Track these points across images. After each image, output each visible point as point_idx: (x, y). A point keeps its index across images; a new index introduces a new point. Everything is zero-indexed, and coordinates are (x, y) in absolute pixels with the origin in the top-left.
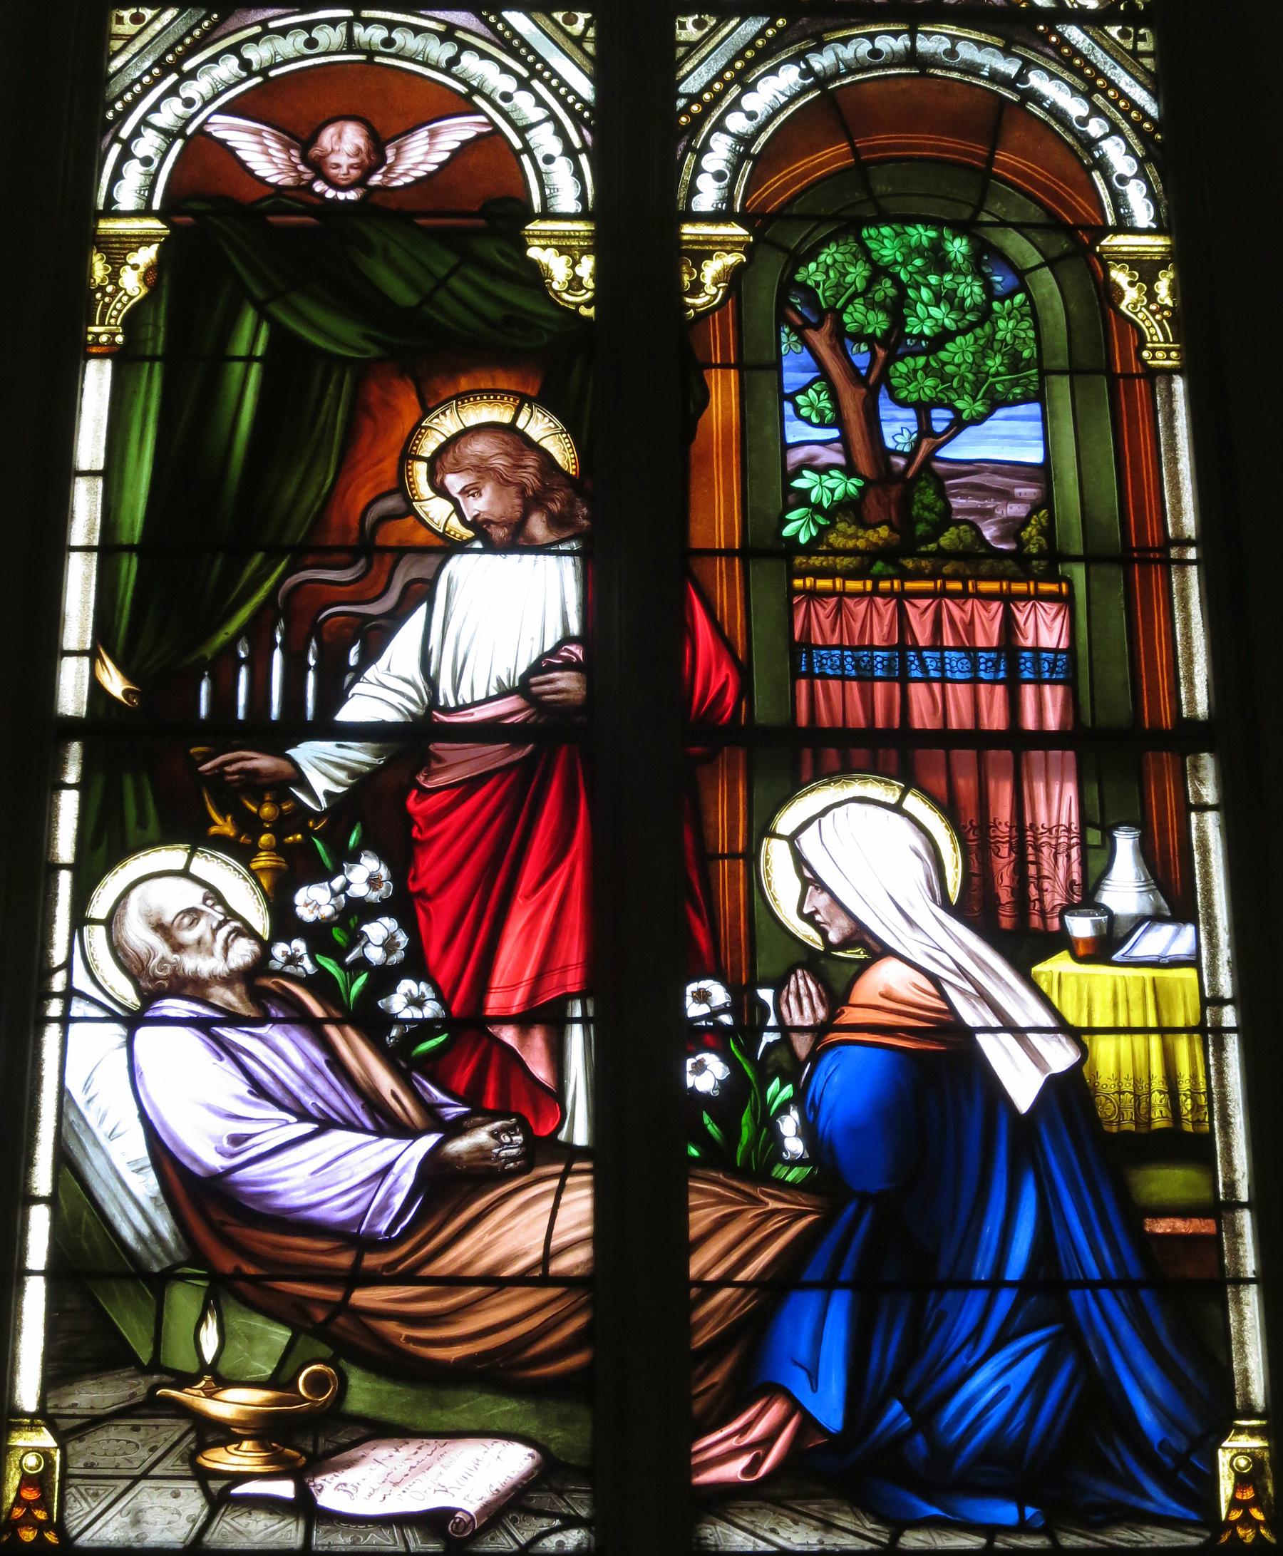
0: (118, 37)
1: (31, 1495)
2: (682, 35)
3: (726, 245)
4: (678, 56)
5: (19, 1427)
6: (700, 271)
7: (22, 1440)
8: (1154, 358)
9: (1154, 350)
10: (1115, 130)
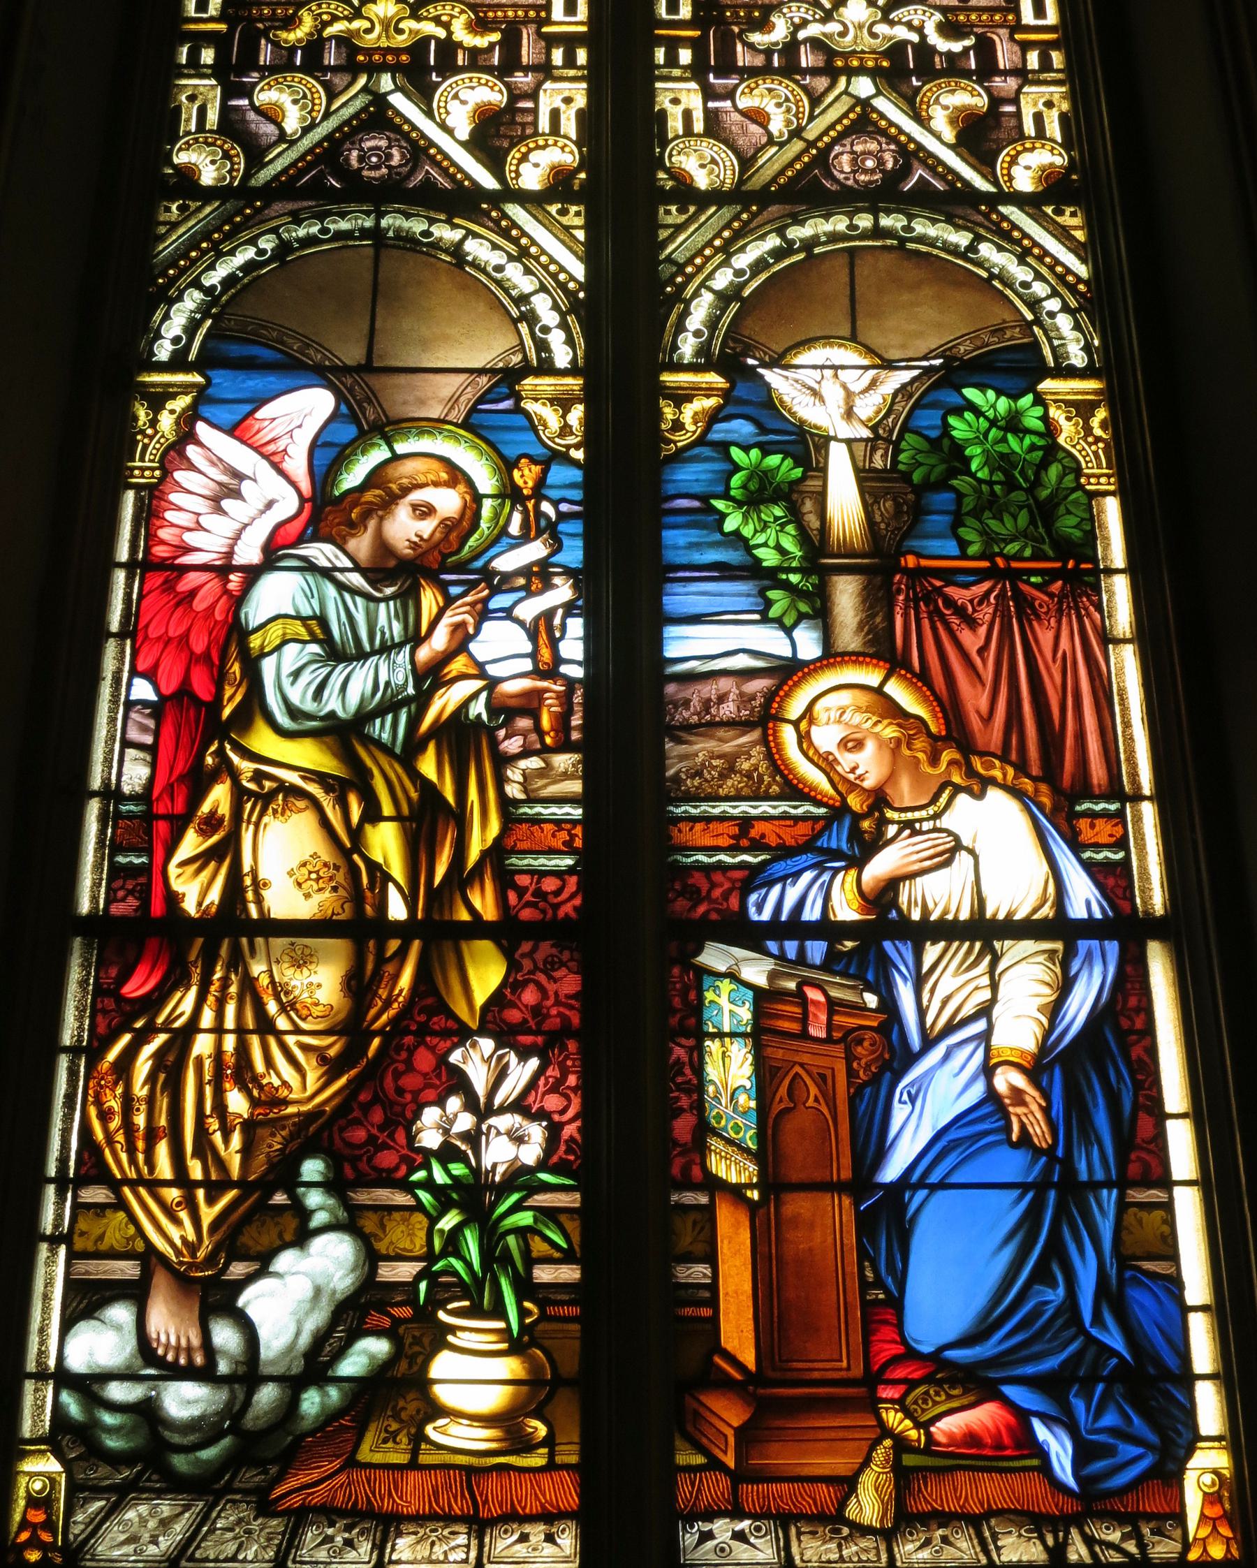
0: (667, 226)
1: (38, 1517)
2: (163, 217)
3: (708, 392)
4: (661, 238)
5: (24, 1455)
6: (681, 413)
7: (29, 1466)
8: (1089, 484)
9: (1089, 476)
10: (543, 288)
